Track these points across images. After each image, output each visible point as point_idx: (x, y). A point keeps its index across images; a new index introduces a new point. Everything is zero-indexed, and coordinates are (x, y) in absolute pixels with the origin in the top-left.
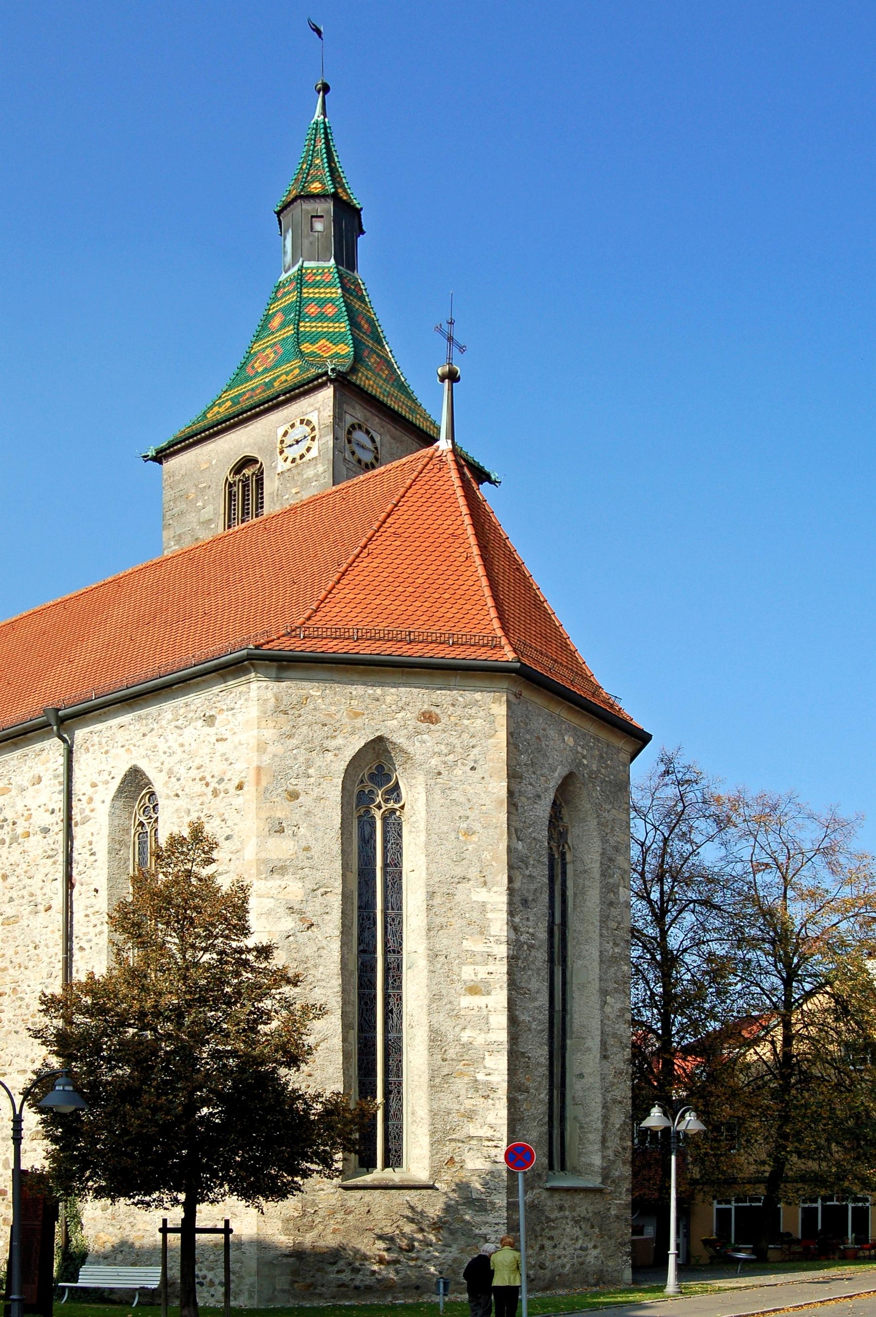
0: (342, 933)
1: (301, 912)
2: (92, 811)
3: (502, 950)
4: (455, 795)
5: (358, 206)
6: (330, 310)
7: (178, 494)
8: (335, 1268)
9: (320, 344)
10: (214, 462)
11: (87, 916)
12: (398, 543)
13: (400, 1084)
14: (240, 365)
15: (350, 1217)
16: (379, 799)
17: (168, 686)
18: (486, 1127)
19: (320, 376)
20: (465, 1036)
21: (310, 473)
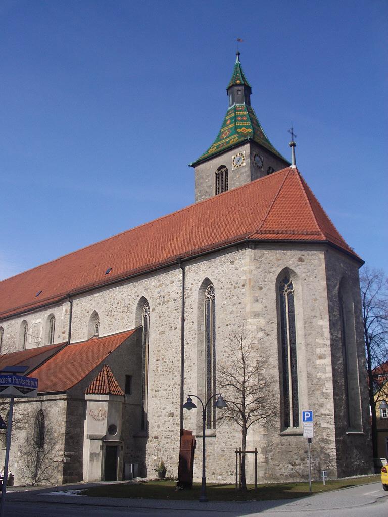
0: (278, 337)
1: (265, 330)
2: (192, 293)
3: (329, 342)
4: (311, 287)
8: (279, 467)
11: (190, 331)
13: (297, 394)
15: (283, 447)
16: (286, 289)
17: (219, 250)
18: (327, 410)
20: (319, 375)
21: (243, 170)
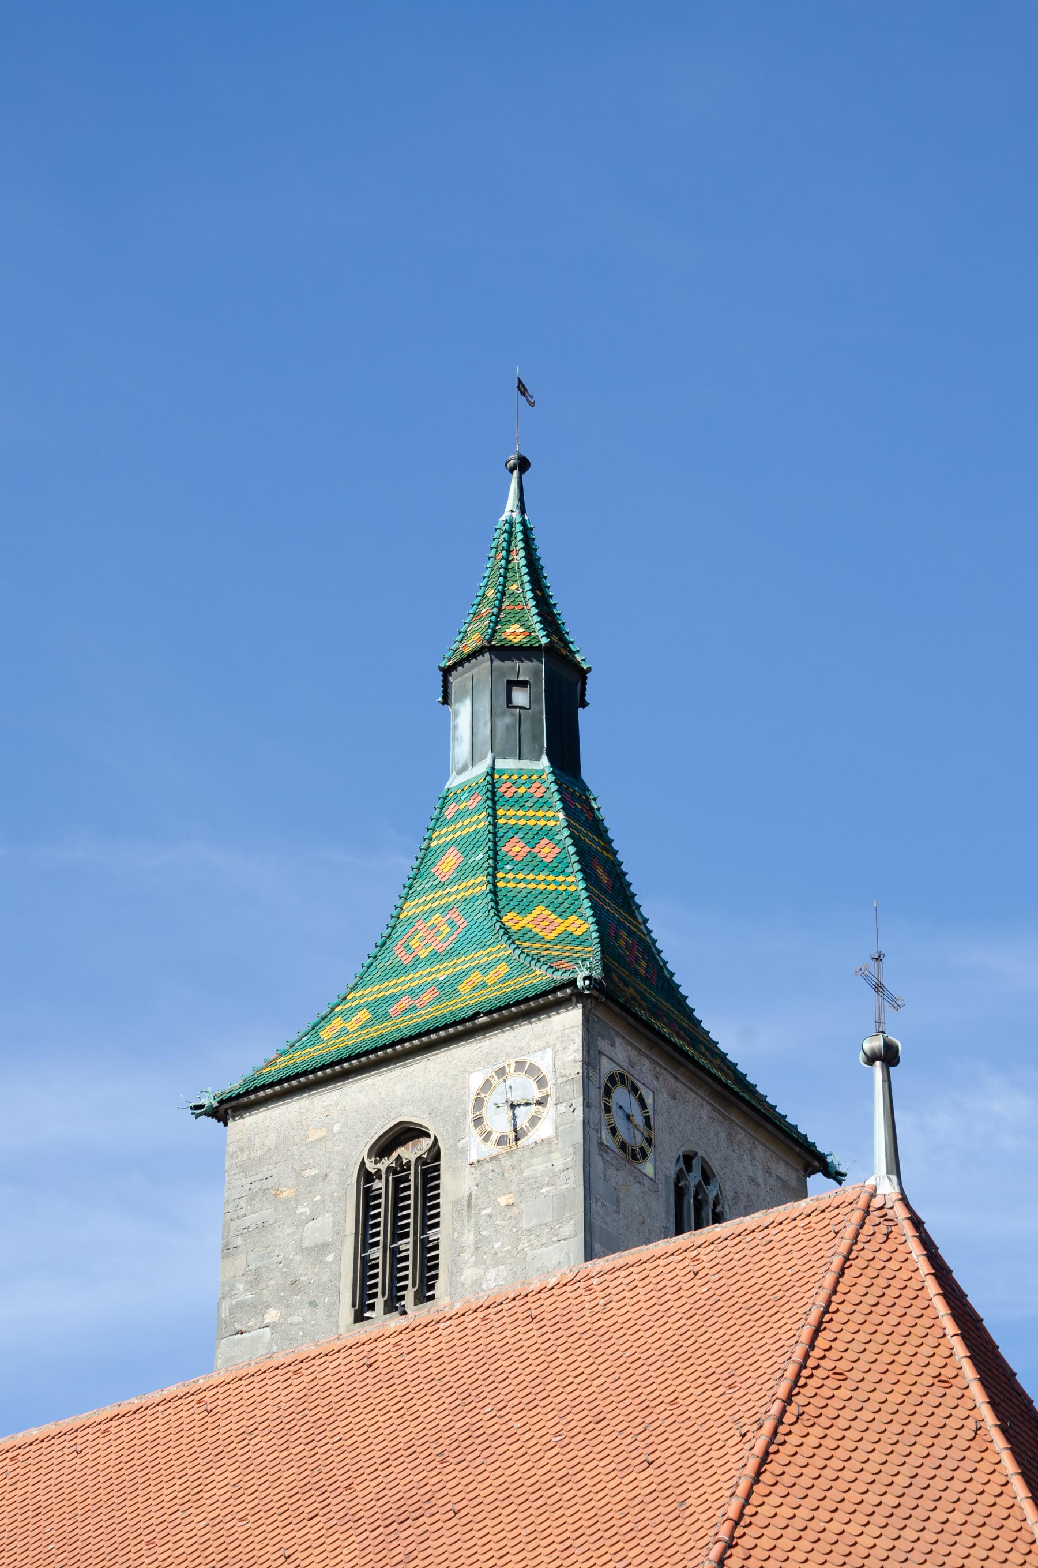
5: (585, 666)
6: (546, 850)
7: (257, 1185)
9: (535, 913)
10: (336, 1128)
12: (843, 1393)
14: (380, 942)
19: (562, 986)
21: (538, 1166)
